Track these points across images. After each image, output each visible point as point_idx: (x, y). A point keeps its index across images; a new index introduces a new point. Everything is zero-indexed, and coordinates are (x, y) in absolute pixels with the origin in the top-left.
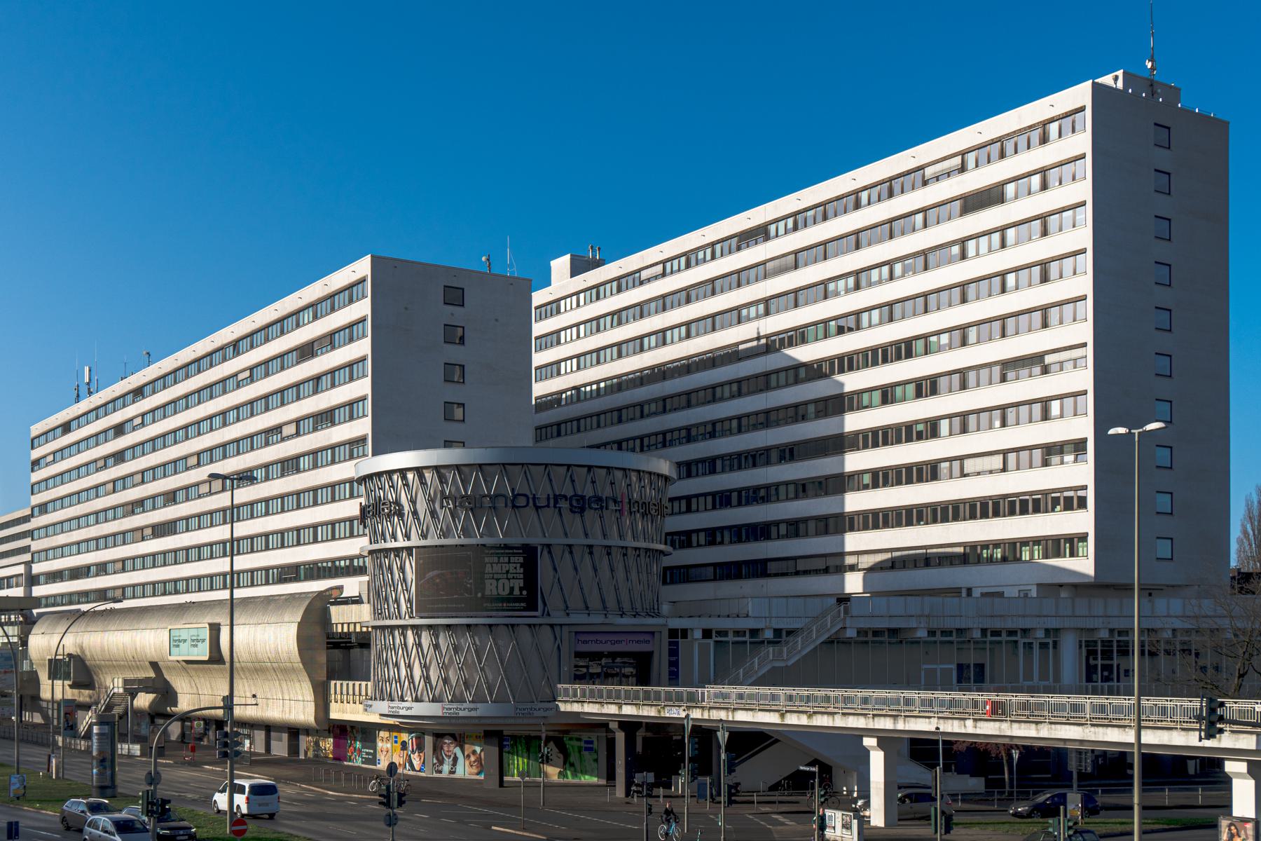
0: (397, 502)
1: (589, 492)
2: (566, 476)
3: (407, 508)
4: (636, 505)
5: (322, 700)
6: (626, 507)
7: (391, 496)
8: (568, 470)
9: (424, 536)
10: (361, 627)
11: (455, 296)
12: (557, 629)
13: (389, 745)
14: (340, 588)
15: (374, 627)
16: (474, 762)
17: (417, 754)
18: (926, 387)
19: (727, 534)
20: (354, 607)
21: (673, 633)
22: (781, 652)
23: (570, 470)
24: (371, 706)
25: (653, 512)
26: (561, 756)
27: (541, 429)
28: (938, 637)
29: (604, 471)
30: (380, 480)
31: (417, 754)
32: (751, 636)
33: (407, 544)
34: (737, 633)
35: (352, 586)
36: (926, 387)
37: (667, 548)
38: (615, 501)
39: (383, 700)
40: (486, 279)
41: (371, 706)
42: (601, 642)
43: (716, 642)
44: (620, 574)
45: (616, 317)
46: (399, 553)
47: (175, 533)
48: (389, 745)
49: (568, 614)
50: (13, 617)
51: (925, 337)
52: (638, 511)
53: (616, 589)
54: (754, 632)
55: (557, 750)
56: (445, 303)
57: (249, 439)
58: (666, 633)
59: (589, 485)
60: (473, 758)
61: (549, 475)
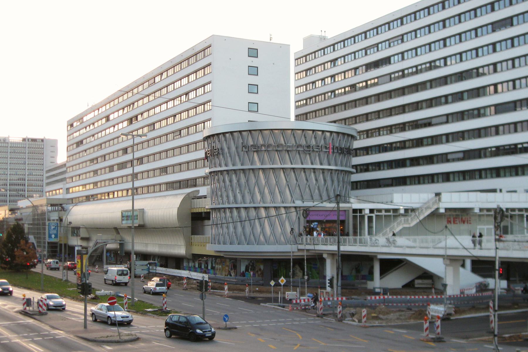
0: (222, 149)
1: (303, 142)
2: (302, 135)
3: (226, 150)
4: (337, 149)
5: (189, 244)
6: (331, 151)
7: (219, 146)
8: (292, 131)
9: (226, 165)
10: (204, 209)
11: (253, 53)
12: (298, 209)
13: (220, 266)
14: (198, 191)
15: (212, 209)
16: (260, 274)
17: (233, 271)
18: (477, 92)
19: (385, 165)
20: (204, 199)
21: (355, 211)
22: (408, 220)
23: (315, 133)
24: (463, 266)
25: (345, 152)
26: (302, 271)
27: (298, 116)
28: (485, 212)
29: (311, 132)
30: (214, 139)
31: (233, 271)
32: (393, 212)
33: (226, 168)
34: (387, 210)
35: (203, 191)
36: (477, 92)
37: (354, 170)
38: (326, 148)
39: (216, 244)
40: (270, 45)
41: (463, 266)
42: (320, 215)
43: (376, 216)
44: (329, 182)
45: (333, 63)
46: (222, 173)
47: (126, 168)
48: (220, 266)
49: (303, 202)
50: (57, 208)
51: (477, 69)
52: (338, 152)
53: (327, 190)
54: (396, 210)
55: (300, 269)
56: (248, 56)
57: (194, 127)
58: (351, 211)
59: (313, 140)
60: (259, 273)
61: (293, 134)
